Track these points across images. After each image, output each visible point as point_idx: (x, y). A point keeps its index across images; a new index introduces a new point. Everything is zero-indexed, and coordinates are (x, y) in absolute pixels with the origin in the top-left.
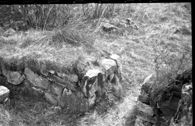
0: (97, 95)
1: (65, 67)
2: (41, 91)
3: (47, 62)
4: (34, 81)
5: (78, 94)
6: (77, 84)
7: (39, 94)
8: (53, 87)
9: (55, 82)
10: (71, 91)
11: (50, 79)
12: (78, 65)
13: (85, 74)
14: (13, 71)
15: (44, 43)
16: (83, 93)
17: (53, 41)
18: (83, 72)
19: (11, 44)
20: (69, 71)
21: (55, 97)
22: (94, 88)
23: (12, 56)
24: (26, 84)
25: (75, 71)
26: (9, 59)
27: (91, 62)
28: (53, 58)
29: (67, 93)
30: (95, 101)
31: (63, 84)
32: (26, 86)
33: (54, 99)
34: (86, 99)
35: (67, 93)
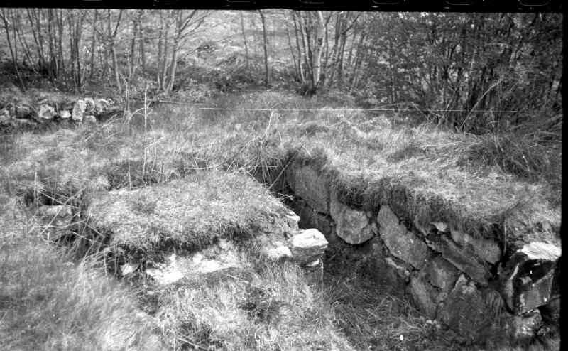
0: (544, 316)
1: (475, 218)
2: (403, 271)
3: (435, 198)
4: (394, 242)
5: (491, 296)
6: (494, 268)
7: (398, 280)
8: (435, 265)
9: (441, 253)
10: (474, 286)
11: (431, 243)
12: (508, 222)
13: (522, 248)
14: (353, 209)
15: (445, 160)
16: (505, 298)
17: (471, 159)
18: (517, 243)
19: (370, 147)
20: (481, 229)
21: (434, 295)
22: (538, 295)
23: (361, 172)
24: (374, 248)
25: (495, 233)
26: (352, 178)
27: (551, 225)
28: (453, 193)
29: (464, 287)
30: (535, 330)
31: (459, 264)
32: (374, 254)
33: (431, 298)
34: (508, 315)
35: (464, 287)
